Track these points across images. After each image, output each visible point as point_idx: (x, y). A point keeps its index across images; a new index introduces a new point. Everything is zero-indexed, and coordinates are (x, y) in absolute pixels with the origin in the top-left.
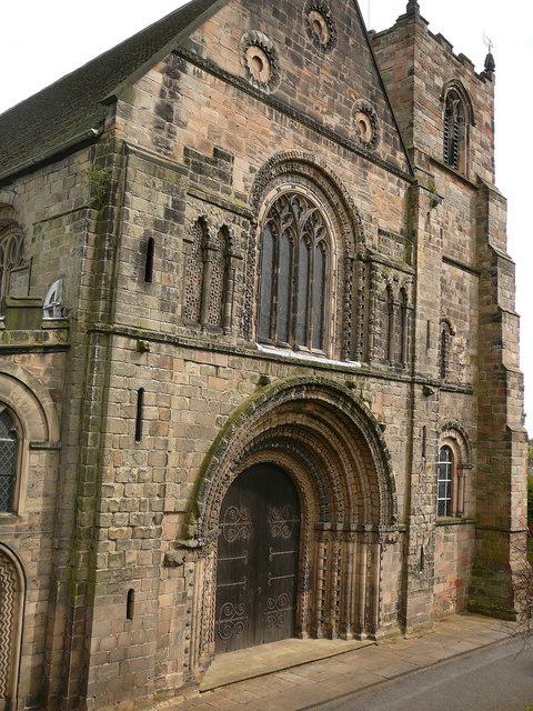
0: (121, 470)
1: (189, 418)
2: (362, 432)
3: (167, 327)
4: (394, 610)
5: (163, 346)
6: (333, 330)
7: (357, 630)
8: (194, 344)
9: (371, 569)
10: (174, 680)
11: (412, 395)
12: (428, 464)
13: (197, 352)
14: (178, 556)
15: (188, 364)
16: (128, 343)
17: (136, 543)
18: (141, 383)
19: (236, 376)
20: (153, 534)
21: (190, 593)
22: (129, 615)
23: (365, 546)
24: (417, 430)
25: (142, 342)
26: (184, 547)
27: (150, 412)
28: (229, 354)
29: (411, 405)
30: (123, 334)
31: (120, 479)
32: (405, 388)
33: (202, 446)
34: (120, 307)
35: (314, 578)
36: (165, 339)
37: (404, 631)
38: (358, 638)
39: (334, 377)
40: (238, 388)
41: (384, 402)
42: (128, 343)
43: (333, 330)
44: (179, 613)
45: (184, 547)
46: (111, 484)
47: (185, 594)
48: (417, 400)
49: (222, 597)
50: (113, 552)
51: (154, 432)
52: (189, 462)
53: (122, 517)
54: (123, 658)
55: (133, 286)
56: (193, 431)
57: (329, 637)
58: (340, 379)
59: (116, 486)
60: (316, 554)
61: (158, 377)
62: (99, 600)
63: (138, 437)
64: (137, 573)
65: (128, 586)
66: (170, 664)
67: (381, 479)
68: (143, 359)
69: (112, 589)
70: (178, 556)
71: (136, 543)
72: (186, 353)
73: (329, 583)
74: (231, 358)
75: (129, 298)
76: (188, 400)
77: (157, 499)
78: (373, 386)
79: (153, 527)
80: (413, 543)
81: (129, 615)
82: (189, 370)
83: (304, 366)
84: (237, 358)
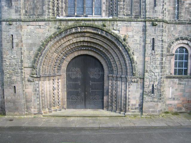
0: (8, 56)
1: (30, 41)
2: (117, 43)
3: (18, 17)
4: (137, 106)
5: (18, 22)
6: (104, 8)
7: (121, 110)
8: (29, 20)
9: (126, 91)
10: (34, 111)
11: (145, 26)
12: (156, 53)
13: (32, 22)
14: (31, 79)
15: (29, 26)
16: (6, 23)
17: (15, 75)
18: (12, 33)
19: (47, 27)
20: (20, 72)
21: (38, 89)
22: (15, 92)
23: (123, 83)
24: (149, 40)
25: (10, 22)
26: (32, 77)
27: (15, 41)
28: (44, 21)
29: (145, 30)
30: (4, 21)
31: (8, 58)
32: (141, 24)
33: (35, 49)
34: (3, 14)
35: (108, 92)
36: (17, 20)
37: (142, 114)
38: (120, 113)
39: (96, 23)
40: (49, 31)
41: (129, 32)
42: (6, 23)
43: (104, 8)
44: (35, 94)
45: (32, 77)
46: (6, 60)
47: (36, 90)
48: (147, 28)
49: (69, 94)
50: (9, 76)
51: (17, 46)
52: (32, 53)
53: (10, 68)
54: (14, 102)
55: (6, 8)
56: (31, 46)
57: (112, 111)
58: (99, 24)
59: (7, 60)
60: (108, 84)
61: (17, 31)
62: (5, 88)
63: (13, 48)
64: (16, 82)
65: (13, 85)
66: (33, 107)
67: (127, 59)
68: (11, 27)
69: (8, 85)
70: (31, 79)
71: (15, 75)
72: (27, 23)
73: (112, 94)
74: (45, 22)
75: (5, 11)
76: (29, 36)
77: (20, 63)
78: (119, 24)
79: (19, 71)
80: (146, 83)
81: (15, 92)
82: (28, 29)
83: (78, 21)
84: (47, 22)
